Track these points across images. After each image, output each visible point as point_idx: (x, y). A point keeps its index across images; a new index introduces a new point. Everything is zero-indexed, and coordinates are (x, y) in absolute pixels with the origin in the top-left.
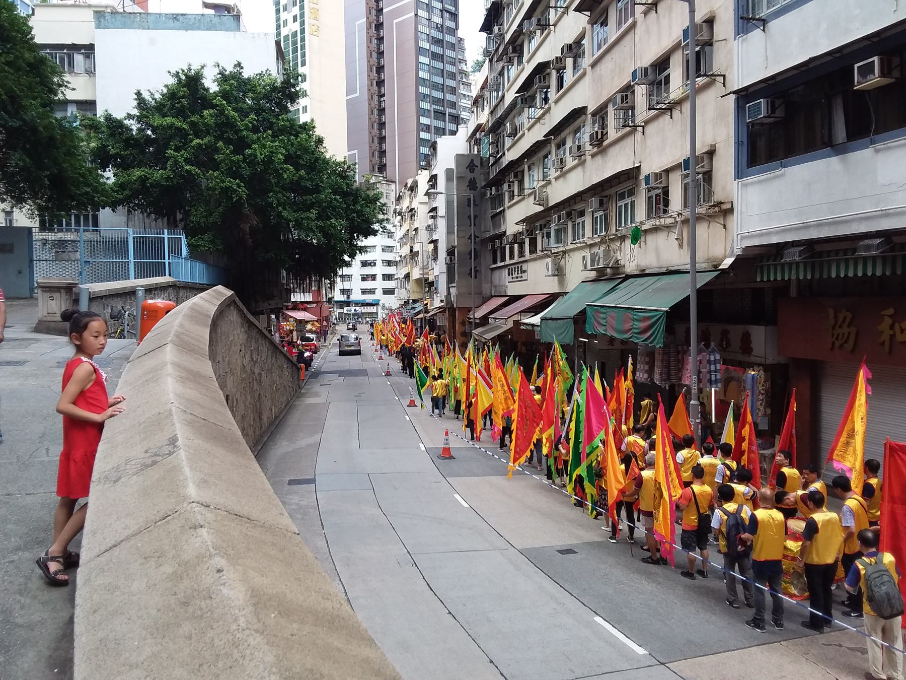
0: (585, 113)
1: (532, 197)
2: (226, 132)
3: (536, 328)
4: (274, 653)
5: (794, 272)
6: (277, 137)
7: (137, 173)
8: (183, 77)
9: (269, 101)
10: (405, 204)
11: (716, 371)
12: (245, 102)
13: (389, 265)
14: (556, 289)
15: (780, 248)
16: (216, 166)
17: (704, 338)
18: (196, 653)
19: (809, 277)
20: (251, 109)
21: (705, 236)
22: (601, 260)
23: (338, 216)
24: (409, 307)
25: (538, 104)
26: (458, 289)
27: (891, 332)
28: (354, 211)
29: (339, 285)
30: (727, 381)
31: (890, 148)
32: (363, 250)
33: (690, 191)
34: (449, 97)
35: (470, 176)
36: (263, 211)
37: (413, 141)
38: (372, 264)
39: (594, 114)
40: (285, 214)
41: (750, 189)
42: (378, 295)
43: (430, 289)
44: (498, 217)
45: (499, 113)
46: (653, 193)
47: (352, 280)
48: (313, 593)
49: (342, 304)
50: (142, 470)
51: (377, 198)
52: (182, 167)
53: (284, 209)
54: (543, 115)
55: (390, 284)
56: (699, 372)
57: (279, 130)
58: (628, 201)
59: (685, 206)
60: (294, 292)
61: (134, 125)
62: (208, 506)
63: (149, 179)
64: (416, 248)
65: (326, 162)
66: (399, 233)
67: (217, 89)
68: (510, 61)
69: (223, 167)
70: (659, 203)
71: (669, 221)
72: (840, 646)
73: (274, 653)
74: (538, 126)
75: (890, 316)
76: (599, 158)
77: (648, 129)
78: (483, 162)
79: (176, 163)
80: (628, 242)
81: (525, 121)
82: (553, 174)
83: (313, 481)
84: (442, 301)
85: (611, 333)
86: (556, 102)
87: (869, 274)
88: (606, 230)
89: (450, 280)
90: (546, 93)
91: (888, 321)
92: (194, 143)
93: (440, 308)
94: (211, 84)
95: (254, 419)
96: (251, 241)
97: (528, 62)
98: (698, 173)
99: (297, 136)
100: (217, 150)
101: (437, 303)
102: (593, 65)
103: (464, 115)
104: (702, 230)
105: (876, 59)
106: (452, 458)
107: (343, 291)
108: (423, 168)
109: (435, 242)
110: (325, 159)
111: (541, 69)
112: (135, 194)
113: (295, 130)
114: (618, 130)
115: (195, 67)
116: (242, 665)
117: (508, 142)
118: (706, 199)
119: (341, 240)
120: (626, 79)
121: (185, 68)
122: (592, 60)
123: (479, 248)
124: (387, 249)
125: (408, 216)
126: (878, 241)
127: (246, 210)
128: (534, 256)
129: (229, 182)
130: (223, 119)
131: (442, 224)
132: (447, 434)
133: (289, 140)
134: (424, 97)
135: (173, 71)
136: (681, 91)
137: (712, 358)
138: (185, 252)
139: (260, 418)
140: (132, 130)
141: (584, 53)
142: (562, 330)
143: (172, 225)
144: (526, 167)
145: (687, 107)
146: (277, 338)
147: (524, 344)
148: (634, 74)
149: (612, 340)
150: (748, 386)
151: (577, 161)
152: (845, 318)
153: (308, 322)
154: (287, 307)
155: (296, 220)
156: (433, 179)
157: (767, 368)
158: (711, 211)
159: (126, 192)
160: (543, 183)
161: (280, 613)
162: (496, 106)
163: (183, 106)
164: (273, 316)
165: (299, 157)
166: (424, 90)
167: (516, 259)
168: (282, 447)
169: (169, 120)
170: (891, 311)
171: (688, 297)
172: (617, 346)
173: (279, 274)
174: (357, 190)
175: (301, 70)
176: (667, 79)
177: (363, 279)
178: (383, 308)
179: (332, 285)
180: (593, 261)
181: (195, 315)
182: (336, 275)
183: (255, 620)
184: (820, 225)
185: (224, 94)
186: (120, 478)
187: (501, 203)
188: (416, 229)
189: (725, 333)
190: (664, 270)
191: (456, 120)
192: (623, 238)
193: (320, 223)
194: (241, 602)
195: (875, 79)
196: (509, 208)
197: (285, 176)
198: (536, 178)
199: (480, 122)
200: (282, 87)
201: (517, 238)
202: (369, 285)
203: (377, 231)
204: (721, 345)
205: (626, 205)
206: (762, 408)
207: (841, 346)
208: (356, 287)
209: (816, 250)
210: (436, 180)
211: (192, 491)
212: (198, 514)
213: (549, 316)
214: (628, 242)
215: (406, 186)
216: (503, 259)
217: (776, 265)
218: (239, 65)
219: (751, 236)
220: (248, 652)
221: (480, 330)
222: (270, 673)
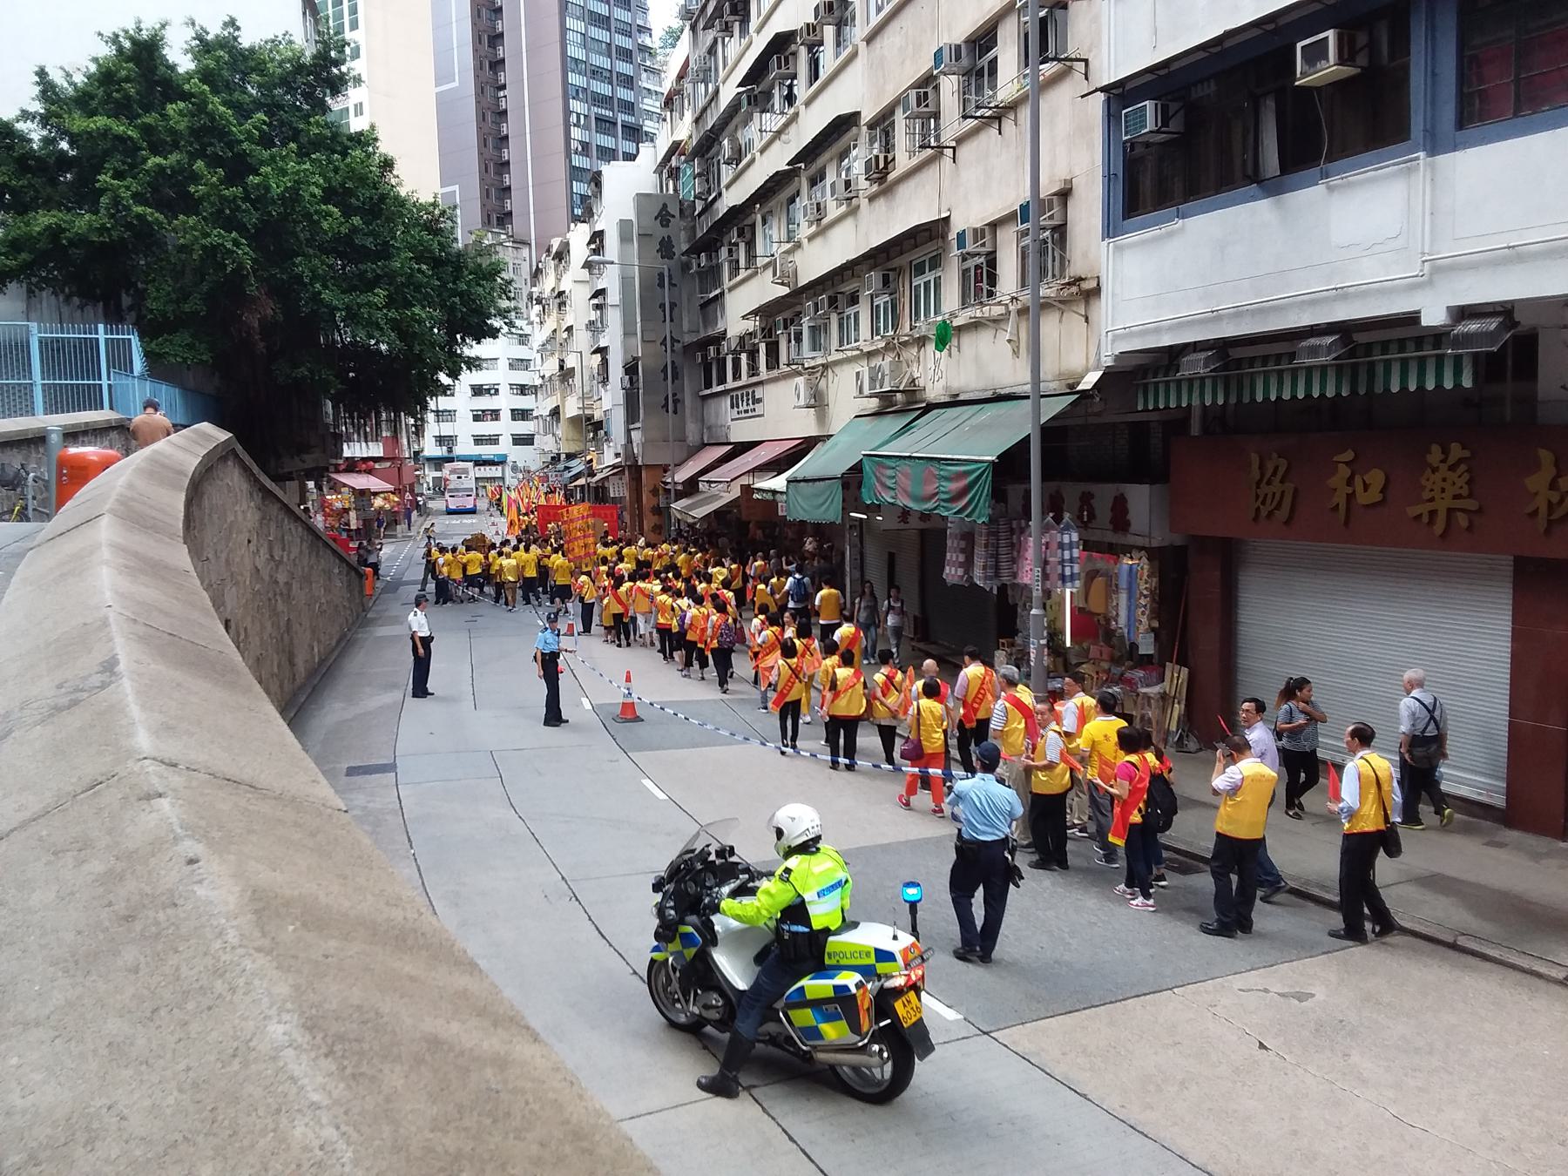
0: (857, 124)
1: (770, 271)
2: (211, 144)
3: (778, 497)
4: (291, 981)
5: (1196, 394)
6: (308, 155)
7: (43, 220)
8: (127, 44)
9: (291, 90)
10: (548, 284)
11: (1071, 560)
12: (245, 91)
13: (523, 393)
14: (812, 431)
15: (1174, 354)
16: (191, 205)
17: (1054, 506)
18: (146, 992)
19: (1220, 402)
20: (258, 105)
21: (1056, 335)
22: (887, 379)
23: (426, 301)
24: (561, 466)
25: (777, 107)
26: (644, 434)
27: (1350, 490)
28: (455, 293)
29: (432, 428)
30: (1091, 576)
31: (1350, 185)
32: (474, 363)
33: (1030, 260)
34: (624, 94)
35: (661, 232)
36: (286, 291)
37: (561, 172)
38: (492, 391)
39: (872, 126)
40: (326, 296)
41: (1128, 256)
42: (505, 447)
43: (596, 434)
44: (711, 306)
45: (711, 121)
46: (971, 263)
47: (456, 416)
48: (369, 897)
49: (438, 463)
50: (52, 715)
51: (495, 271)
52: (127, 208)
53: (325, 287)
54: (786, 125)
55: (524, 428)
56: (1046, 562)
57: (310, 142)
58: (930, 276)
59: (1023, 285)
60: (349, 440)
61: (35, 133)
62: (175, 765)
63: (64, 230)
64: (571, 362)
65: (401, 203)
66: (539, 336)
67: (192, 66)
68: (727, 29)
69: (207, 209)
70: (981, 279)
71: (997, 311)
72: (1266, 991)
73: (291, 981)
74: (777, 145)
75: (1346, 463)
76: (881, 202)
77: (961, 152)
78: (685, 209)
79: (116, 201)
80: (931, 347)
81: (756, 136)
82: (804, 230)
83: (392, 767)
84: (617, 455)
85: (903, 501)
86: (808, 103)
87: (1316, 394)
88: (895, 327)
89: (631, 416)
90: (790, 87)
91: (1345, 472)
92: (150, 163)
93: (614, 467)
94: (179, 56)
95: (279, 666)
96: (262, 345)
97: (758, 31)
98: (1044, 229)
99: (344, 154)
100: (195, 178)
101: (609, 459)
102: (870, 40)
103: (649, 126)
104: (1050, 325)
105: (1330, 34)
106: (637, 719)
107: (440, 440)
108: (576, 219)
109: (602, 351)
110: (397, 197)
111: (781, 43)
112: (41, 259)
113: (341, 144)
114: (912, 153)
115: (149, 24)
116: (231, 1002)
117: (727, 173)
118: (1057, 272)
119: (433, 345)
120: (925, 65)
121: (131, 27)
122: (867, 31)
123: (684, 363)
124: (518, 364)
125: (554, 304)
126: (1329, 340)
127: (253, 288)
128: (775, 373)
129: (217, 236)
130: (204, 120)
131: (614, 318)
132: (628, 679)
133: (330, 162)
134: (579, 93)
135: (108, 33)
136: (1016, 86)
137: (1066, 539)
138: (138, 364)
139: (292, 664)
140: (30, 141)
141: (853, 19)
142: (821, 500)
143: (114, 317)
144: (759, 217)
145: (1025, 113)
146: (319, 521)
147: (759, 525)
148: (938, 56)
149: (905, 513)
150: (1123, 584)
151: (844, 208)
152: (1276, 469)
153: (376, 494)
154: (337, 466)
155: (348, 308)
156: (597, 237)
157: (1153, 554)
158: (1066, 293)
159: (24, 256)
160: (788, 246)
161: (304, 925)
162: (704, 110)
163: (128, 97)
164: (311, 484)
165: (349, 193)
166: (574, 79)
167: (744, 380)
168: (333, 712)
169: (101, 121)
170: (1349, 455)
171: (1026, 440)
172: (914, 523)
173: (319, 406)
174: (459, 254)
175: (348, 35)
176: (993, 63)
177: (476, 418)
178: (515, 469)
179: (419, 431)
180: (872, 380)
181: (160, 471)
182: (425, 407)
183: (257, 934)
184: (1238, 314)
185: (206, 75)
186: (10, 732)
187: (718, 282)
188: (569, 329)
189: (1086, 499)
190: (989, 394)
191: (635, 133)
192: (921, 342)
193: (392, 314)
194: (232, 907)
195: (1330, 69)
196: (730, 290)
197: (325, 225)
198: (775, 239)
199: (677, 138)
200: (315, 65)
201: (746, 344)
202: (487, 428)
203: (498, 330)
204: (1080, 517)
205: (927, 284)
206: (1144, 619)
207: (1270, 514)
208: (464, 431)
209: (1233, 356)
210: (602, 241)
211: (143, 741)
212: (154, 776)
213: (800, 477)
214: (931, 347)
215: (548, 251)
216: (722, 381)
217: (1167, 383)
218: (232, 23)
219: (1129, 334)
220: (241, 981)
221: (684, 502)
222: (281, 1010)
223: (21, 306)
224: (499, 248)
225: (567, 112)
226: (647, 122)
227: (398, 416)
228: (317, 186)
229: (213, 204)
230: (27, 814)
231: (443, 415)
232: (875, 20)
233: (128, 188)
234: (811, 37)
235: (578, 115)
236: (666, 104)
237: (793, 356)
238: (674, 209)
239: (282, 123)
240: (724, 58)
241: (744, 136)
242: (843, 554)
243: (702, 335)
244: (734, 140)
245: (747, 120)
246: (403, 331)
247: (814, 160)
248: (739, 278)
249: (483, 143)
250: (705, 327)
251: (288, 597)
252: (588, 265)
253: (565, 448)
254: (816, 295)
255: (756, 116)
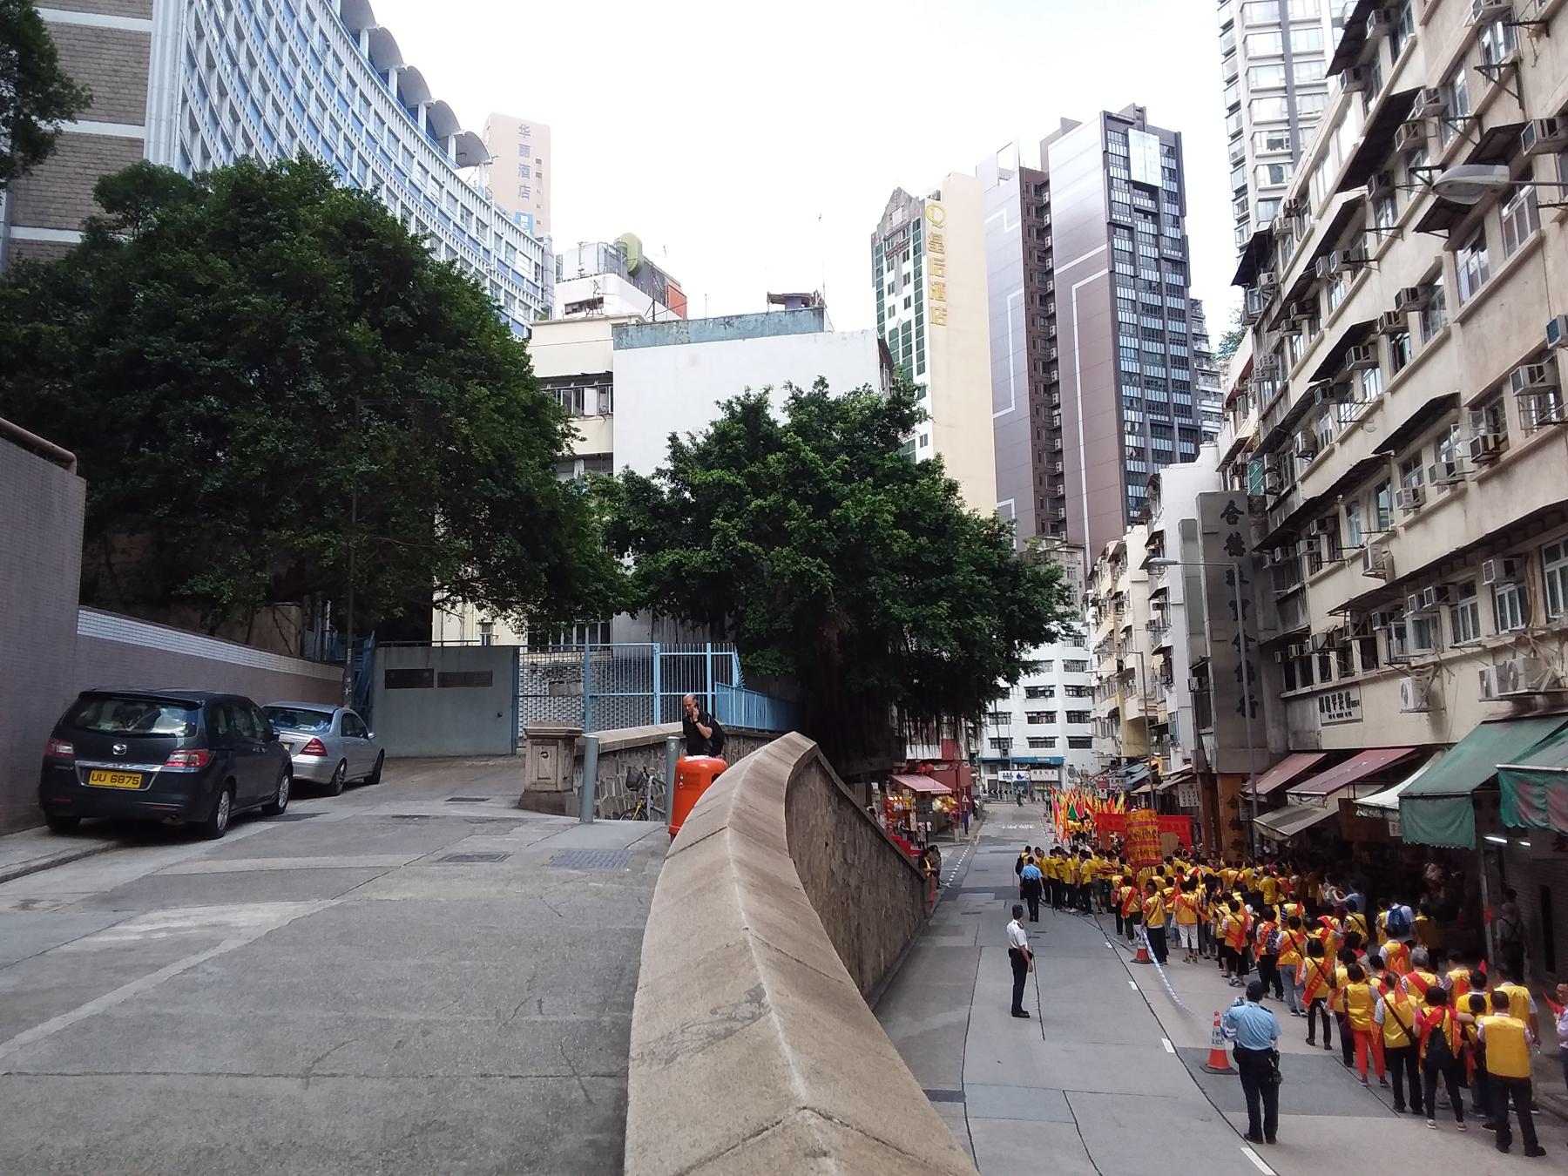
1: (1360, 563)
3: (1389, 815)
7: (669, 557)
8: (739, 409)
9: (869, 433)
10: (1104, 586)
12: (830, 437)
14: (1425, 737)
16: (784, 538)
20: (841, 447)
22: (1522, 680)
23: (986, 610)
24: (1122, 771)
28: (1013, 601)
29: (991, 731)
32: (1032, 667)
35: (1227, 529)
37: (1114, 476)
38: (1047, 692)
39: (1474, 406)
40: (895, 610)
42: (1060, 749)
44: (1291, 603)
47: (1012, 720)
49: (993, 765)
50: (710, 1043)
51: (1053, 577)
52: (734, 544)
53: (894, 602)
61: (665, 486)
62: (830, 1118)
64: (1130, 662)
65: (964, 521)
66: (1095, 637)
67: (789, 421)
69: (797, 540)
74: (1359, 434)
78: (1256, 505)
79: (725, 537)
82: (1399, 518)
84: (1186, 761)
88: (1526, 618)
93: (1183, 773)
97: (1331, 325)
99: (914, 483)
100: (788, 514)
101: (1177, 765)
102: (1464, 320)
103: (1208, 426)
108: (1133, 522)
109: (1165, 651)
110: (960, 517)
114: (1528, 431)
119: (992, 651)
121: (741, 394)
122: (1460, 312)
124: (1073, 665)
125: (1110, 606)
127: (833, 606)
128: (1373, 673)
129: (806, 563)
130: (797, 465)
131: (1178, 618)
134: (1133, 403)
135: (724, 401)
141: (1442, 301)
142: (1448, 820)
143: (718, 637)
144: (1342, 509)
153: (935, 796)
155: (914, 620)
156: (1156, 539)
160: (1379, 536)
162: (1272, 406)
163: (737, 452)
164: (875, 786)
165: (918, 516)
167: (1335, 679)
173: (885, 713)
174: (1018, 564)
177: (1031, 720)
178: (1072, 772)
179: (976, 734)
180: (1502, 680)
181: (760, 780)
185: (798, 428)
191: (1194, 435)
196: (1312, 584)
197: (896, 548)
198: (1364, 528)
202: (1042, 730)
203: (1056, 634)
208: (1019, 733)
210: (1161, 541)
211: (799, 1086)
213: (1416, 791)
215: (1104, 554)
216: (1308, 680)
218: (822, 382)
223: (647, 629)
224: (1054, 555)
225: (1121, 421)
226: (1206, 423)
227: (958, 720)
228: (890, 512)
229: (802, 536)
230: (699, 1153)
231: (997, 717)
232: (1469, 301)
233: (734, 527)
234: (1394, 325)
235: (1133, 423)
236: (1228, 404)
237: (1395, 653)
238: (1241, 506)
239: (861, 462)
240: (1293, 356)
241: (1318, 429)
242: (1478, 885)
243: (1281, 632)
244: (1308, 433)
245: (1324, 410)
246: (965, 639)
247: (1404, 447)
248: (1322, 572)
249: (1037, 458)
250: (1284, 620)
251: (858, 902)
252: (1146, 565)
253: (1126, 752)
254: (1419, 587)
255: (1333, 407)
